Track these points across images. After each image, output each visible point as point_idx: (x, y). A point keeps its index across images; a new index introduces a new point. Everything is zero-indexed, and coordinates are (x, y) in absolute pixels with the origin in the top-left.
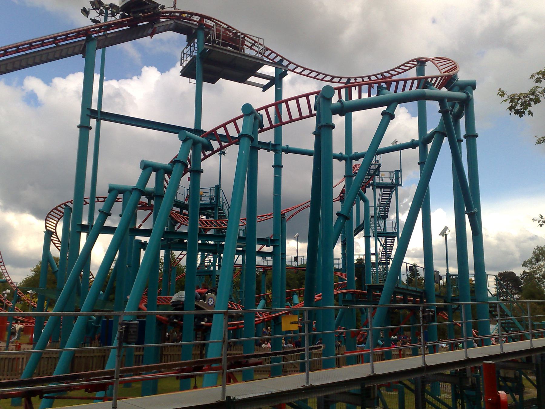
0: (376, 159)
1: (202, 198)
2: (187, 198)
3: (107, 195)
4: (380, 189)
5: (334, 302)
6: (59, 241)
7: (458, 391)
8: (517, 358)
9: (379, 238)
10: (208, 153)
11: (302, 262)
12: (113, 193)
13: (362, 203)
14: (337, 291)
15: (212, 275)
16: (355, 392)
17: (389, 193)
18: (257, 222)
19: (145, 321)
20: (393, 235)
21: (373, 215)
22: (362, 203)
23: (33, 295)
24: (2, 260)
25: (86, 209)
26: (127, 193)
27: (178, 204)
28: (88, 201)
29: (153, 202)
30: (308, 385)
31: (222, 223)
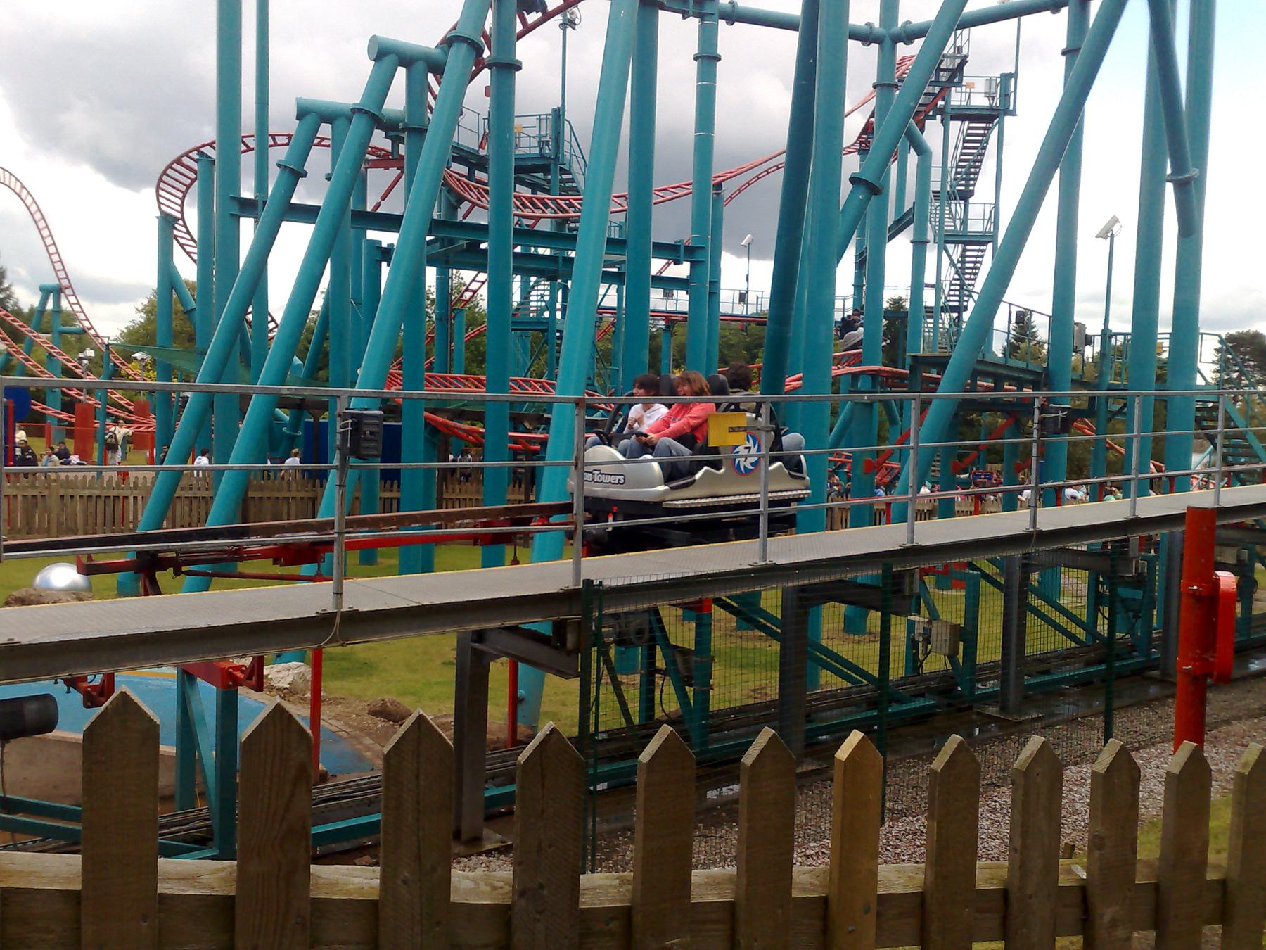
0: (955, 42)
1: (519, 140)
2: (484, 141)
3: (292, 126)
4: (960, 122)
5: (829, 387)
6: (193, 239)
7: (1104, 589)
8: (1249, 520)
9: (947, 245)
10: (532, 17)
11: (757, 304)
12: (309, 119)
13: (913, 158)
14: (839, 369)
15: (546, 330)
16: (869, 582)
17: (982, 132)
18: (655, 204)
19: (400, 426)
20: (981, 240)
21: (939, 189)
22: (913, 158)
23: (146, 365)
24: (69, 282)
25: (248, 162)
26: (341, 122)
27: (462, 156)
28: (251, 143)
29: (402, 149)
30: (763, 563)
31: (571, 205)
